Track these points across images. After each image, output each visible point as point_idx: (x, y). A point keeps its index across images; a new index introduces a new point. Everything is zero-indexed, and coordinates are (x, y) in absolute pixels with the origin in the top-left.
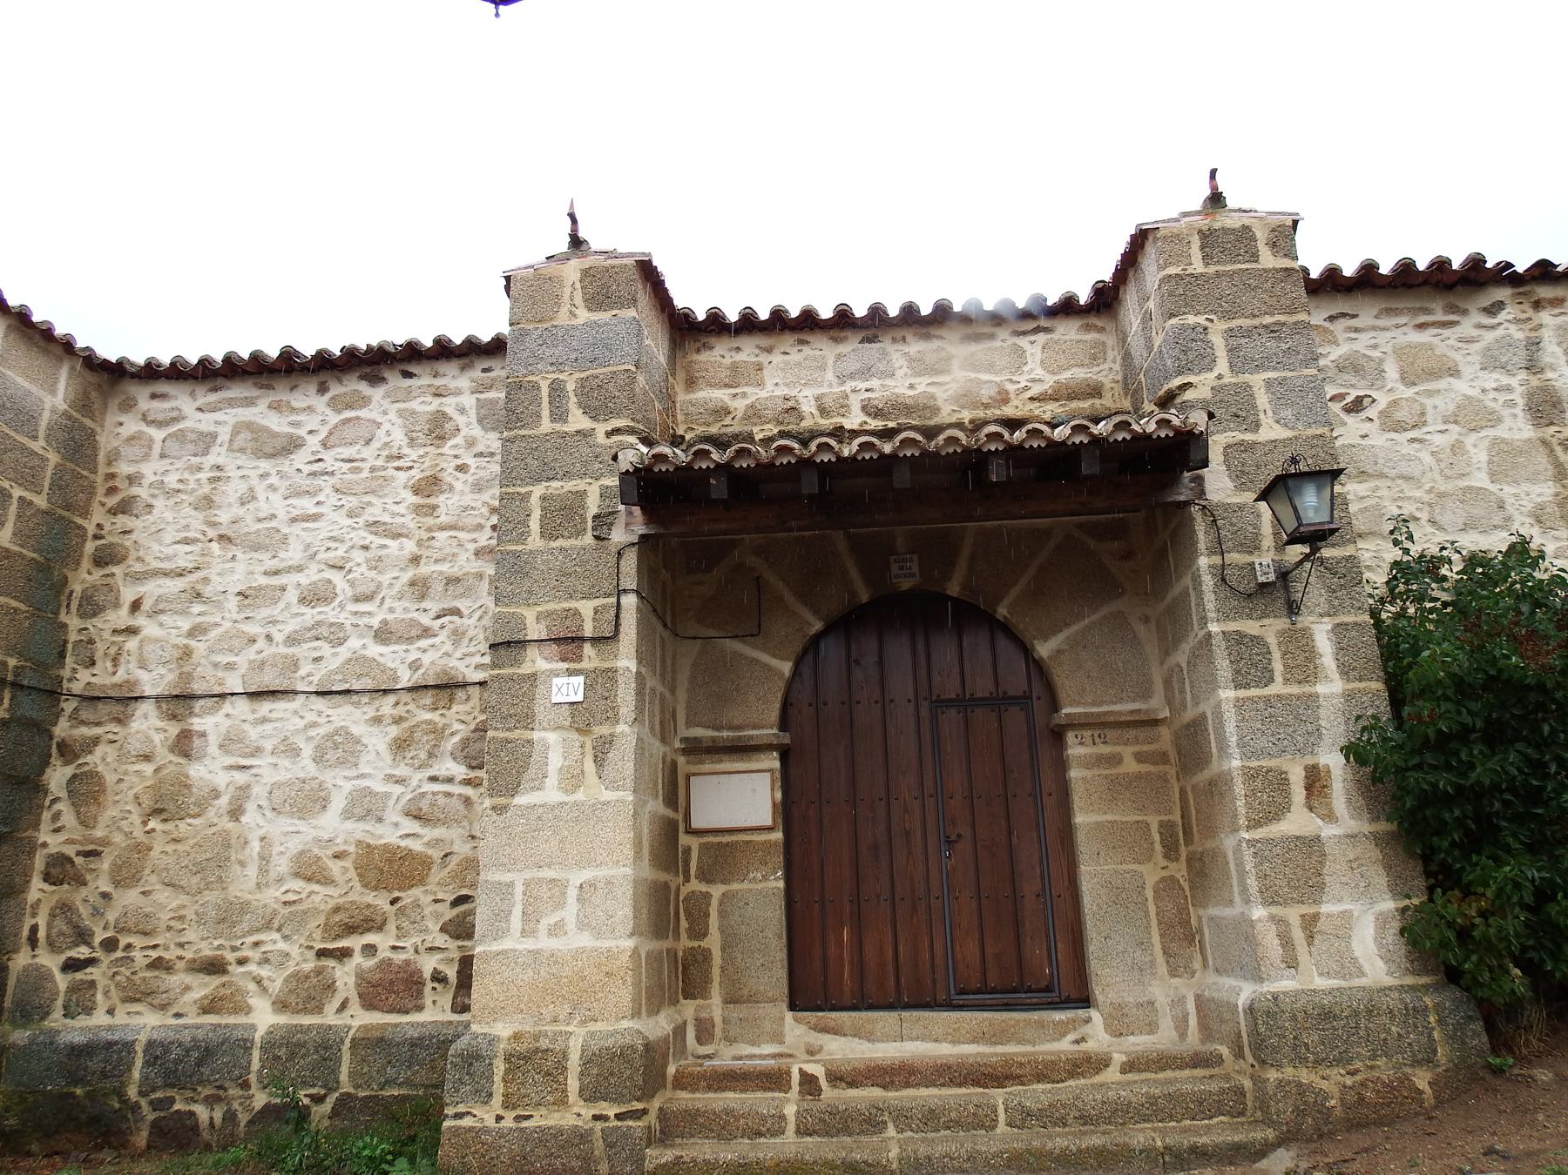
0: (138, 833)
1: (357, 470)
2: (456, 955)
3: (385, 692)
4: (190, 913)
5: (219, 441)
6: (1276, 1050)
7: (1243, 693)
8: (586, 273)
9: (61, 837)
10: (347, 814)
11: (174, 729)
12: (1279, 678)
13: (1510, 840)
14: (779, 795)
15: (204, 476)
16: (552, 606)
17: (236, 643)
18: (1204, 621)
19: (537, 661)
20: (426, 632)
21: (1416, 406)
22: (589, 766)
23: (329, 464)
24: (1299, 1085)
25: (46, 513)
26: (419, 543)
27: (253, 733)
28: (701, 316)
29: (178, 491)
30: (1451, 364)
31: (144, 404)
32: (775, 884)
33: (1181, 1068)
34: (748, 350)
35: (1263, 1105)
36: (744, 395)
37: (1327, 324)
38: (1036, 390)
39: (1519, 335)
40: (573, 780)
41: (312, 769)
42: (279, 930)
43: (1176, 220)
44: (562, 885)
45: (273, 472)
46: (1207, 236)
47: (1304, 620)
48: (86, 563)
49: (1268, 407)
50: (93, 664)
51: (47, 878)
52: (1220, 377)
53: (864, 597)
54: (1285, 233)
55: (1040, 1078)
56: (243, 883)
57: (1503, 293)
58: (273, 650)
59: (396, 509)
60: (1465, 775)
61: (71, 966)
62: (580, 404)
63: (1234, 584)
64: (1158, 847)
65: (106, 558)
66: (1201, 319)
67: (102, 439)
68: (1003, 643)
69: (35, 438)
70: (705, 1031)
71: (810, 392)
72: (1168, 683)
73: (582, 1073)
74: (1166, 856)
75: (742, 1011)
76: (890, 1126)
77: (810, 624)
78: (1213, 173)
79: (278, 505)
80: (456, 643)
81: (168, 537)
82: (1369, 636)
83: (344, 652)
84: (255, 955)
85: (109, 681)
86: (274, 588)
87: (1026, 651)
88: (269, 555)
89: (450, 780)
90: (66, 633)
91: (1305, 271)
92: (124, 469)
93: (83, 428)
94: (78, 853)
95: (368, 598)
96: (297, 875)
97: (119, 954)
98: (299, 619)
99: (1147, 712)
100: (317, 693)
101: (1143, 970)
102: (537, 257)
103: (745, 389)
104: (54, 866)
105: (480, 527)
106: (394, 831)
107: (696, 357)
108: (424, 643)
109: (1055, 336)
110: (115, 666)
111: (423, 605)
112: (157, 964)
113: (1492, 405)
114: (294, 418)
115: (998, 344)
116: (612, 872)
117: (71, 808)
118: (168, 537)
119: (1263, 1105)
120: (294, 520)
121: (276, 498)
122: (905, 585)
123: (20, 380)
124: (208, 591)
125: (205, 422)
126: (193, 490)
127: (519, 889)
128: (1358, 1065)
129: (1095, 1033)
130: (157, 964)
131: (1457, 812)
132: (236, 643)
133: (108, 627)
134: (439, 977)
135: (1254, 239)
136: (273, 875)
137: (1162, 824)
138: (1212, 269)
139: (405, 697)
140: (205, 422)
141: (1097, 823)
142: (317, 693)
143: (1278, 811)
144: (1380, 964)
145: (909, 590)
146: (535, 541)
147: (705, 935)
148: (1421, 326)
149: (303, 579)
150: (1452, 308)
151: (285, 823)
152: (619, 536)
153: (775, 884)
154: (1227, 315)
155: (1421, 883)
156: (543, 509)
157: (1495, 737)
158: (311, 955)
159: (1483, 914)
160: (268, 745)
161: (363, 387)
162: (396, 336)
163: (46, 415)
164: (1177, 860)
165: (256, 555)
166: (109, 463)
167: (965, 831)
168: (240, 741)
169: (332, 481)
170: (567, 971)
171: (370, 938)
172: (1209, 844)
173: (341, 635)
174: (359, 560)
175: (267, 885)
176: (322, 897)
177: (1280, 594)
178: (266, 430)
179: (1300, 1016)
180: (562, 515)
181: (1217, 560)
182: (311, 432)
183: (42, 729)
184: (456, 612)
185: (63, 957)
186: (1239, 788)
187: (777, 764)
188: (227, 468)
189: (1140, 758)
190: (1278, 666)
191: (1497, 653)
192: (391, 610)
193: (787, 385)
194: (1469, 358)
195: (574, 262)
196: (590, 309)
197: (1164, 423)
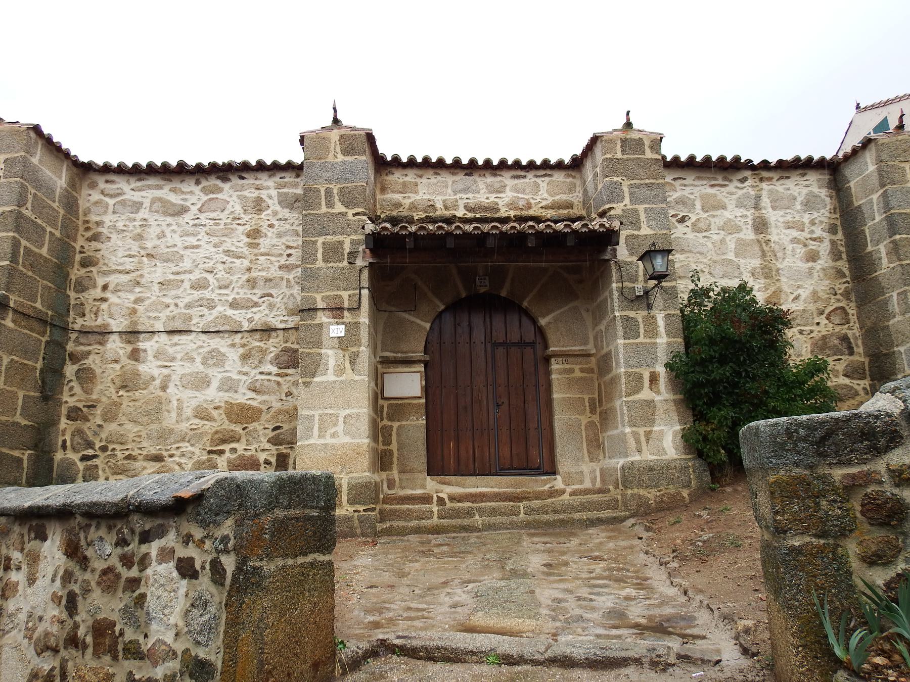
0: (114, 397)
1: (218, 224)
2: (275, 453)
3: (237, 332)
4: (143, 434)
5: (144, 206)
6: (631, 482)
7: (627, 341)
8: (341, 137)
9: (75, 399)
10: (220, 389)
11: (129, 348)
12: (642, 336)
13: (725, 402)
14: (424, 383)
15: (137, 223)
16: (328, 293)
17: (159, 307)
18: (613, 311)
19: (323, 318)
20: (256, 304)
21: (707, 222)
22: (347, 365)
23: (203, 220)
24: (639, 495)
25: (60, 239)
26: (251, 261)
27: (171, 350)
28: (389, 158)
29: (124, 231)
30: (723, 204)
31: (102, 185)
32: (421, 422)
33: (594, 494)
34: (410, 176)
35: (625, 504)
36: (409, 197)
37: (672, 182)
38: (544, 203)
39: (753, 193)
40: (340, 371)
41: (201, 368)
42: (189, 442)
43: (611, 133)
44: (337, 417)
45: (174, 223)
46: (624, 142)
47: (654, 312)
48: (76, 265)
49: (645, 220)
50: (84, 315)
51: (69, 417)
52: (625, 205)
53: (464, 295)
54: (657, 142)
55: (537, 498)
56: (169, 420)
57: (748, 173)
58: (179, 311)
59: (238, 244)
60: (710, 376)
61: (84, 458)
62: (340, 200)
63: (626, 295)
64: (588, 408)
65: (87, 263)
66: (619, 179)
67: (80, 202)
68: (525, 320)
69: (54, 201)
70: (391, 484)
71: (440, 198)
72: (596, 338)
73: (348, 493)
74: (591, 412)
75: (404, 476)
76: (477, 514)
77: (439, 306)
78: (628, 113)
79: (177, 239)
80: (271, 310)
81: (120, 254)
82: (679, 320)
83: (215, 313)
84: (178, 453)
85: (93, 324)
86: (178, 281)
87: (534, 322)
88: (174, 265)
89: (270, 374)
90: (69, 300)
91: (664, 157)
92: (93, 218)
93: (73, 197)
94: (84, 406)
95: (226, 287)
96: (196, 417)
97: (109, 453)
98: (191, 296)
99: (586, 350)
100: (202, 332)
101: (579, 459)
102: (317, 126)
103: (409, 195)
104: (72, 412)
105: (281, 255)
106: (243, 397)
107: (385, 178)
108: (255, 310)
109: (554, 179)
110: (96, 317)
111: (254, 291)
112: (128, 457)
113: (739, 223)
114: (184, 196)
115: (527, 180)
116: (359, 411)
117: (79, 385)
118: (120, 254)
119: (625, 504)
120: (186, 248)
121: (176, 237)
122: (482, 290)
123: (47, 172)
124: (143, 281)
125: (136, 196)
126: (132, 231)
127: (317, 418)
128: (662, 488)
129: (558, 483)
130: (128, 457)
131: (706, 390)
132: (159, 307)
133: (91, 298)
134: (267, 462)
135: (643, 144)
136: (184, 416)
137: (589, 399)
138: (625, 157)
139: (247, 335)
140: (136, 196)
141: (563, 398)
142: (202, 332)
143: (638, 389)
144: (673, 450)
145: (484, 293)
146: (320, 263)
147: (390, 444)
148: (712, 186)
149: (192, 277)
150: (725, 179)
151: (190, 393)
152: (360, 262)
153: (421, 422)
154: (631, 178)
155: (691, 419)
156: (324, 248)
157: (723, 361)
158: (205, 453)
159: (713, 430)
160: (179, 356)
161: (219, 183)
162: (238, 158)
163: (58, 190)
164: (595, 414)
165: (167, 264)
166: (85, 215)
167: (505, 400)
168: (164, 354)
169: (205, 229)
170: (339, 453)
171: (233, 445)
172: (609, 405)
173: (213, 304)
174: (221, 269)
175: (182, 421)
176: (208, 427)
177: (645, 301)
178: (169, 202)
179: (641, 469)
180: (331, 253)
181: (620, 285)
182: (193, 204)
183: (62, 346)
184: (271, 295)
185: (80, 455)
186: (623, 380)
187: (423, 369)
188: (149, 220)
189: (582, 370)
190: (642, 331)
191: (726, 327)
192: (238, 293)
193: (429, 194)
194: (731, 202)
195: (335, 131)
196: (344, 155)
197: (602, 225)
